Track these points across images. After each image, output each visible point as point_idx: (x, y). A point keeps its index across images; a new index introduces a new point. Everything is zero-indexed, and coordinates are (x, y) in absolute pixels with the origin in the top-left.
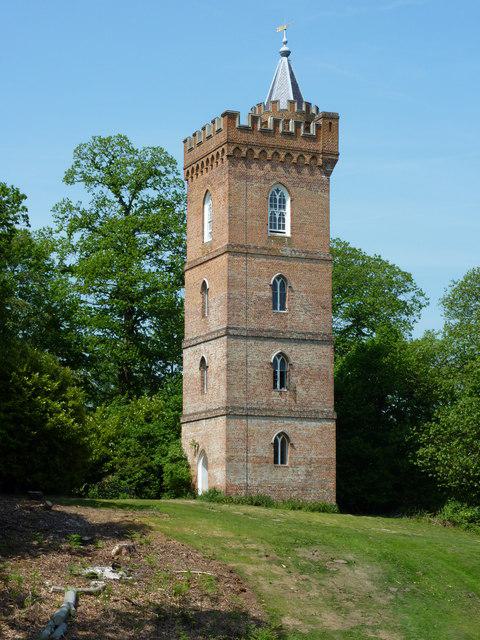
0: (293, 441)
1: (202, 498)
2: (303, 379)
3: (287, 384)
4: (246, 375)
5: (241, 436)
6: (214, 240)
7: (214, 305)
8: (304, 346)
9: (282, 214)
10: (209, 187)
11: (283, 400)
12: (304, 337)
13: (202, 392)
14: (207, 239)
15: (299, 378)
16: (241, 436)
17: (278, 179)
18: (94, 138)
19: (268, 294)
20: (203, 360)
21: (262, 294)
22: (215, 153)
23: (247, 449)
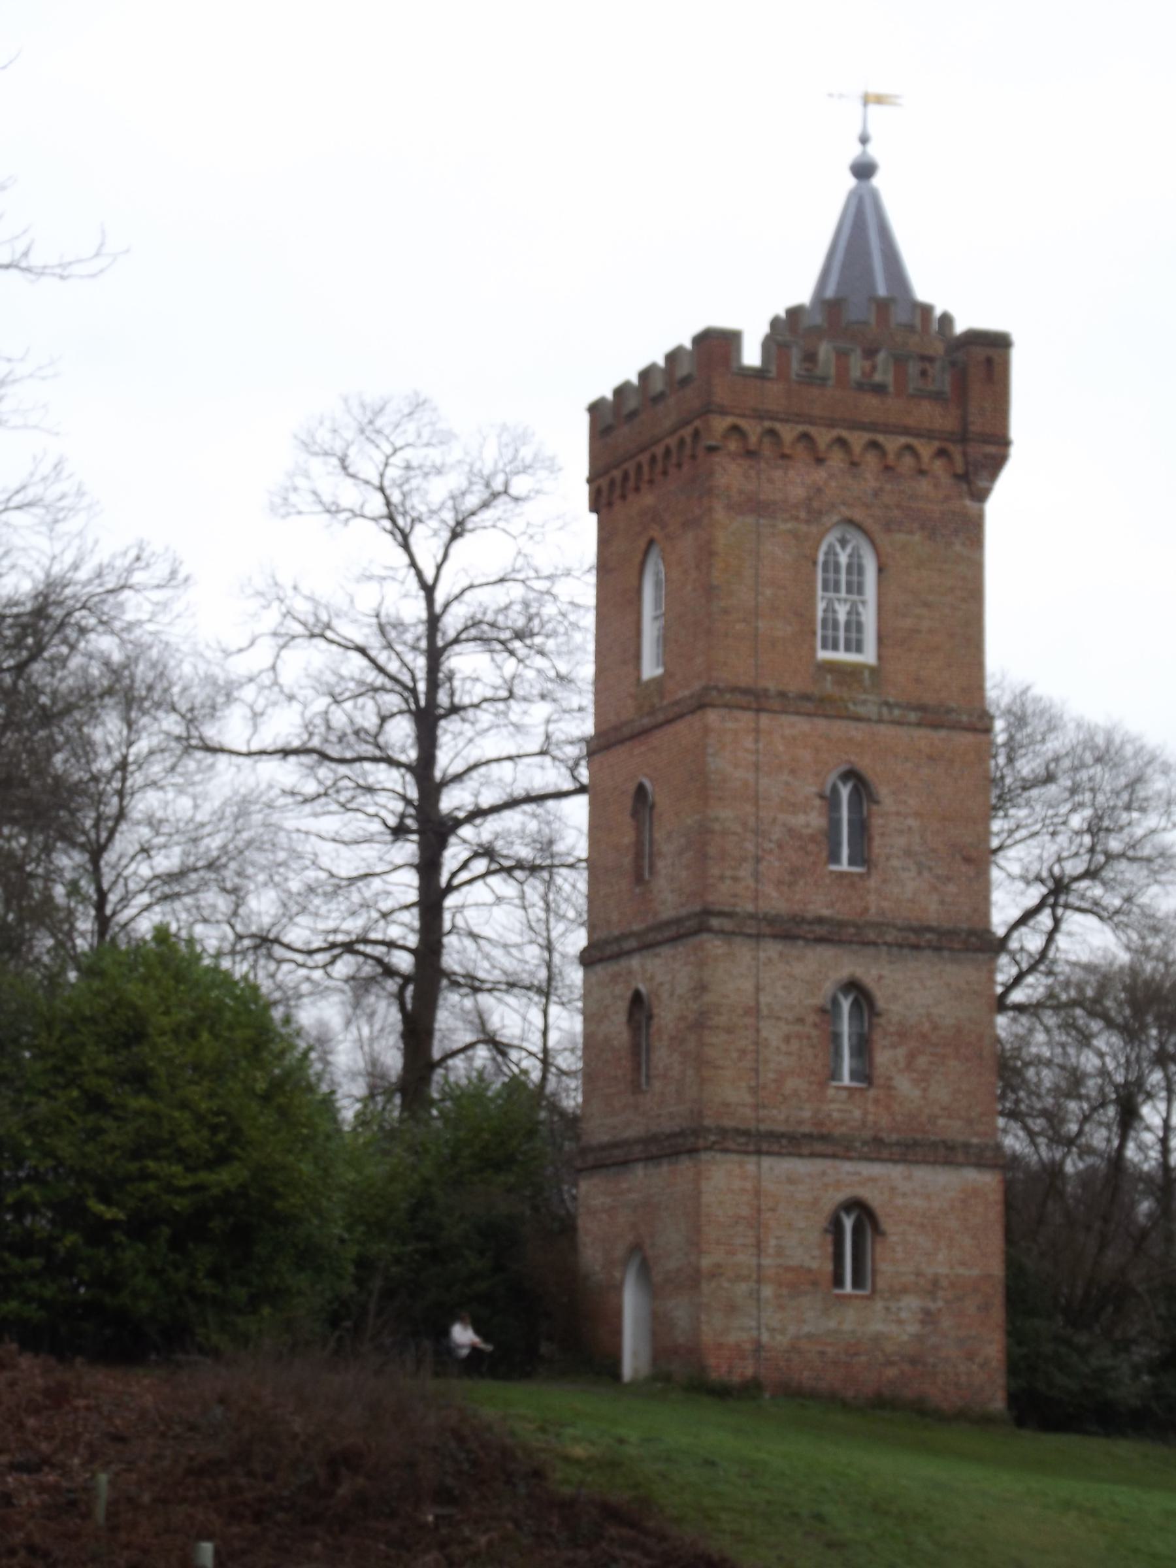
0: (886, 1224)
1: (637, 1389)
2: (911, 1056)
3: (122, 582)
4: (756, 1043)
5: (745, 1211)
6: (668, 674)
7: (667, 848)
8: (551, 789)
9: (853, 612)
10: (655, 532)
11: (857, 1114)
12: (913, 938)
13: (636, 1088)
14: (650, 669)
15: (901, 1052)
16: (745, 1211)
17: (846, 512)
18: (167, 549)
19: (815, 820)
20: (637, 999)
21: (799, 820)
22: (672, 441)
23: (759, 1246)
